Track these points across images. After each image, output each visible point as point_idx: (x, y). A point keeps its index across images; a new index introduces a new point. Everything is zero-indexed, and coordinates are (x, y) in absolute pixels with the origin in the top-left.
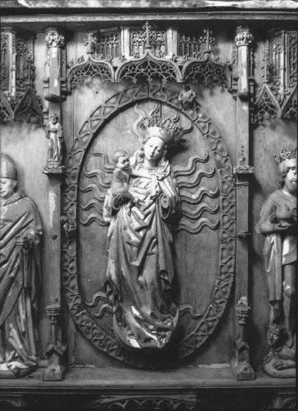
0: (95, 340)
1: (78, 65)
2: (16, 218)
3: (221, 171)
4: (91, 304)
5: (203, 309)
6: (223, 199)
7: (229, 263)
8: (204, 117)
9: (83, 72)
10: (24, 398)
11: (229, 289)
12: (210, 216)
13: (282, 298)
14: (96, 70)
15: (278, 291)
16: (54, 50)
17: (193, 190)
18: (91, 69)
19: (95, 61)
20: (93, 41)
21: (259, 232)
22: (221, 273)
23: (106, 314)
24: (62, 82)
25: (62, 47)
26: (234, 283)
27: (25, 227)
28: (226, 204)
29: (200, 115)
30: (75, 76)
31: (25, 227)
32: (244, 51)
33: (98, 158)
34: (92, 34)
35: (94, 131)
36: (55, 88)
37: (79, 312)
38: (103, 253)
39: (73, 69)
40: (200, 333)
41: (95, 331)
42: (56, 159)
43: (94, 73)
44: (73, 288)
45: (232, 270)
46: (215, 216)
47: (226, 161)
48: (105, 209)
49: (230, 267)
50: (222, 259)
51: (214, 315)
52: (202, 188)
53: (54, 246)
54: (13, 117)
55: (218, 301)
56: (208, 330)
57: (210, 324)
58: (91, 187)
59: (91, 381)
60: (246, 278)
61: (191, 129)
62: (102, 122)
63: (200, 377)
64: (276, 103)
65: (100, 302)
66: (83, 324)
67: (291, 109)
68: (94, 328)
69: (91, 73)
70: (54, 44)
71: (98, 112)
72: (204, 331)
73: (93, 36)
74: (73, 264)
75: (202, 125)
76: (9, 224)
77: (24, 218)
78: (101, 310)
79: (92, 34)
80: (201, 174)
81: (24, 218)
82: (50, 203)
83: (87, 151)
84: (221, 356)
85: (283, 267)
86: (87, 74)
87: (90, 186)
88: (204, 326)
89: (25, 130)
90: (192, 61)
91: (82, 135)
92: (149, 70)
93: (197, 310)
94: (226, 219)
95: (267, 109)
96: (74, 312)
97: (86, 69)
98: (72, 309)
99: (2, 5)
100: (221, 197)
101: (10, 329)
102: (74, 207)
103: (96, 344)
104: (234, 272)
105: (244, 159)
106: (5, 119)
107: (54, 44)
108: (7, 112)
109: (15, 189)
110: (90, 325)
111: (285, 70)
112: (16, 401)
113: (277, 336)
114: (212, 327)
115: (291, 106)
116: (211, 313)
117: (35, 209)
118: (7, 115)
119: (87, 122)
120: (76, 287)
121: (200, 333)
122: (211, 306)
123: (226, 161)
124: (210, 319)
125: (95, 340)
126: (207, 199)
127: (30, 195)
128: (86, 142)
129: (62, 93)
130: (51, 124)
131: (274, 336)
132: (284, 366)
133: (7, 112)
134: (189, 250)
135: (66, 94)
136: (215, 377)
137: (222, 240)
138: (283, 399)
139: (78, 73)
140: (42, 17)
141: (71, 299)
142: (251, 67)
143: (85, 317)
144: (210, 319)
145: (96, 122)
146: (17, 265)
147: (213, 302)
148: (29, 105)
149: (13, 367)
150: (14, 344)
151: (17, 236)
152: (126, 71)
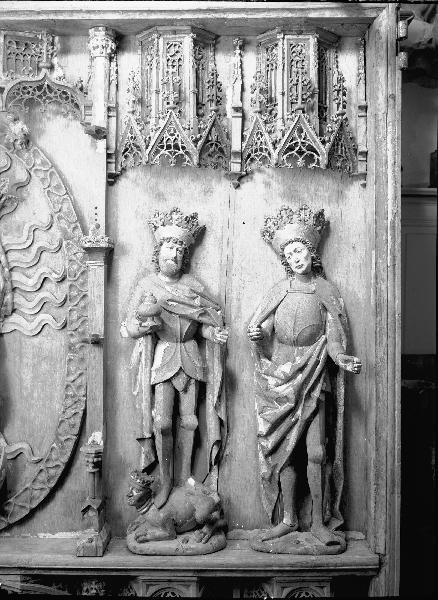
3: (68, 244)
5: (45, 449)
6: (71, 286)
7: (79, 381)
8: (43, 163)
11: (78, 420)
12: (54, 311)
13: (153, 437)
15: (146, 423)
17: (31, 271)
21: (127, 336)
22: (67, 396)
26: (85, 411)
28: (74, 293)
29: (38, 162)
32: (101, 63)
40: (38, 486)
45: (83, 392)
46: (61, 310)
47: (74, 229)
49: (79, 387)
50: (68, 375)
51: (56, 460)
52: (41, 271)
55: (63, 439)
56: (49, 481)
57: (52, 472)
59: (167, 546)
60: (100, 403)
61: (29, 181)
63: (24, 551)
64: (142, 145)
67: (163, 152)
72: (43, 483)
75: (42, 175)
80: (39, 248)
84: (70, 519)
85: (153, 388)
88: (43, 474)
89: (171, 180)
90: (18, 81)
93: (36, 451)
94: (75, 316)
95: (300, 153)
99: (7, 6)
100: (69, 283)
104: (85, 395)
105: (98, 226)
111: (283, 94)
113: (139, 490)
114: (53, 477)
115: (162, 147)
116: (54, 456)
118: (188, 159)
121: (38, 486)
122: (54, 445)
123: (74, 229)
124: (50, 465)
126: (47, 285)
131: (134, 492)
132: (148, 537)
134: (25, 360)
136: (53, 551)
137: (70, 348)
142: (113, 83)
144: (50, 465)
147: (57, 439)
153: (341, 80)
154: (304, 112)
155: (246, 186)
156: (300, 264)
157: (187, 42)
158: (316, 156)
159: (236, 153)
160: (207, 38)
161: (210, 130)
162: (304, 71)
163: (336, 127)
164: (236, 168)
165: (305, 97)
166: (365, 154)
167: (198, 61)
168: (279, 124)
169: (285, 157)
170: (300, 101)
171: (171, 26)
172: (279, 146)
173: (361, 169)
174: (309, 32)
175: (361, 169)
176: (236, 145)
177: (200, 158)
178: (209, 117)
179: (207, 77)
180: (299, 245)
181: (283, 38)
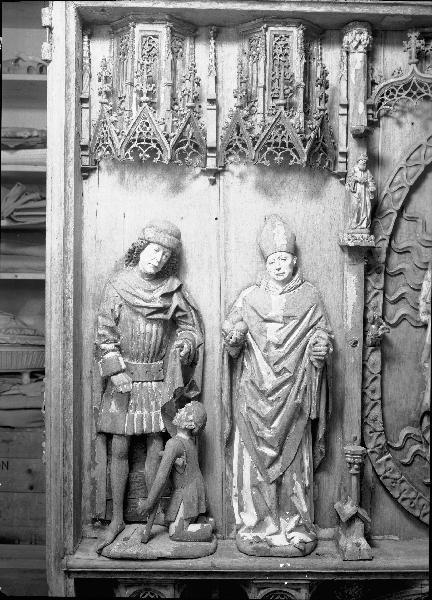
0: (404, 499)
1: (392, 80)
2: (302, 314)
4: (398, 445)
9: (401, 91)
10: (177, 584)
14: (423, 90)
16: (358, 59)
18: (414, 88)
19: (423, 75)
20: (418, 45)
23: (417, 460)
24: (369, 107)
25: (370, 55)
27: (312, 327)
30: (385, 97)
31: (312, 327)
33: (412, 223)
34: (417, 34)
35: (412, 182)
36: (359, 119)
37: (381, 456)
38: (416, 369)
39: (385, 86)
41: (404, 485)
42: (364, 225)
43: (420, 94)
44: (374, 420)
48: (422, 303)
53: (351, 359)
54: (305, 158)
58: (404, 269)
62: (422, 169)
65: (408, 443)
66: (387, 474)
68: (403, 481)
69: (415, 93)
70: (361, 48)
71: (416, 153)
73: (419, 38)
74: (377, 384)
76: (292, 323)
77: (311, 312)
78: (411, 454)
79: (417, 34)
81: (311, 312)
82: (345, 288)
83: (400, 212)
86: (409, 94)
87: (400, 267)
91: (394, 188)
92: (415, 93)
96: (375, 456)
97: (406, 87)
98: (372, 452)
101: (293, 483)
102: (380, 298)
103: (405, 504)
106: (292, 162)
107: (361, 48)
108: (295, 151)
109: (295, 269)
110: (397, 475)
112: (298, 590)
117: (320, 303)
118: (295, 156)
119: (401, 168)
120: (380, 419)
125: (404, 499)
127: (311, 279)
128: (399, 200)
129: (370, 123)
130: (357, 169)
133: (295, 151)
135: (373, 124)
138: (259, 590)
139: (391, 94)
140: (227, 11)
141: (371, 438)
143: (391, 464)
145: (412, 171)
146: (304, 384)
148: (189, 139)
149: (296, 541)
150: (297, 505)
151: (71, 345)
152: (383, 100)
153: (325, 74)
154: (285, 109)
155: (226, 179)
156: (281, 271)
157: (296, 34)
158: (159, 151)
159: (212, 149)
160: (320, 31)
161: (185, 127)
162: (286, 64)
163: (316, 123)
164: (211, 163)
165: (287, 91)
166: (345, 155)
167: (307, 54)
168: (258, 118)
169: (128, 152)
170: (282, 95)
171: (151, 16)
172: (172, 141)
173: (341, 168)
174: (162, 21)
175: (341, 168)
176: (211, 141)
177: (308, 159)
178: (183, 108)
179: (182, 72)
180: (284, 255)
181: (266, 30)
